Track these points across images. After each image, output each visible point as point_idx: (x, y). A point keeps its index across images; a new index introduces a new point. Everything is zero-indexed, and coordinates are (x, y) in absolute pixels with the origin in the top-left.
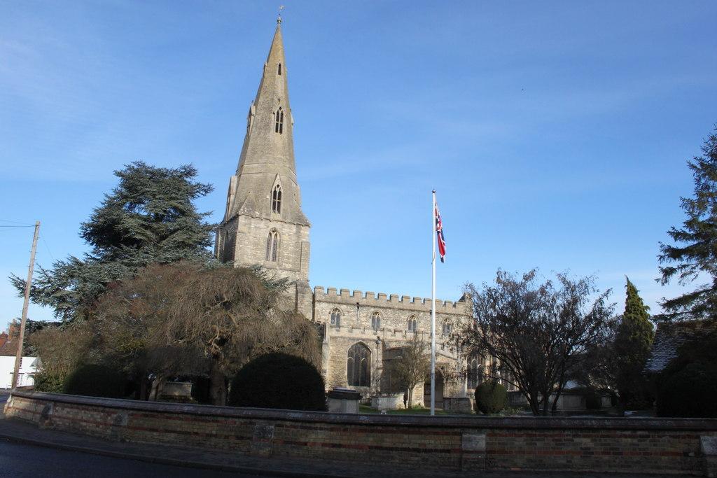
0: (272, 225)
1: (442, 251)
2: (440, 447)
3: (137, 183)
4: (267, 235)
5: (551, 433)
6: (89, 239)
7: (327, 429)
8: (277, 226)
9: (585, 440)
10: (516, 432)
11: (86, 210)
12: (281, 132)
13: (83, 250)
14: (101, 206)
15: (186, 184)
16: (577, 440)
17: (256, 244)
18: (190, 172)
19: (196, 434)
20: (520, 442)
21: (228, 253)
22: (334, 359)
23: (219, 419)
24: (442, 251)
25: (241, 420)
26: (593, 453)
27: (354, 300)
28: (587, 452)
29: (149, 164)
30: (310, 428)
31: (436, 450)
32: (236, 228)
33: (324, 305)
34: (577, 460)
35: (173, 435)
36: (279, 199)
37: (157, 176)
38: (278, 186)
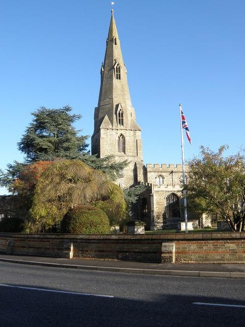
0: (119, 132)
1: (189, 140)
2: (151, 251)
3: (43, 121)
4: (117, 138)
5: (211, 241)
6: (23, 151)
7: (97, 243)
8: (123, 132)
9: (231, 245)
10: (228, 241)
11: (19, 134)
12: (120, 79)
13: (21, 158)
14: (25, 133)
15: (67, 115)
16: (227, 245)
17: (111, 144)
18: (68, 109)
19: (41, 248)
20: (193, 246)
21: (96, 149)
22: (158, 203)
23: (49, 240)
24: (189, 140)
25: (59, 240)
26: (237, 252)
27: (170, 170)
28: (234, 252)
29: (47, 108)
30: (89, 243)
31: (149, 252)
32: (100, 136)
33: (153, 173)
34: (227, 256)
35: (32, 249)
36: (122, 117)
37: (52, 115)
38: (121, 110)
